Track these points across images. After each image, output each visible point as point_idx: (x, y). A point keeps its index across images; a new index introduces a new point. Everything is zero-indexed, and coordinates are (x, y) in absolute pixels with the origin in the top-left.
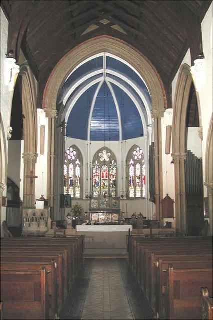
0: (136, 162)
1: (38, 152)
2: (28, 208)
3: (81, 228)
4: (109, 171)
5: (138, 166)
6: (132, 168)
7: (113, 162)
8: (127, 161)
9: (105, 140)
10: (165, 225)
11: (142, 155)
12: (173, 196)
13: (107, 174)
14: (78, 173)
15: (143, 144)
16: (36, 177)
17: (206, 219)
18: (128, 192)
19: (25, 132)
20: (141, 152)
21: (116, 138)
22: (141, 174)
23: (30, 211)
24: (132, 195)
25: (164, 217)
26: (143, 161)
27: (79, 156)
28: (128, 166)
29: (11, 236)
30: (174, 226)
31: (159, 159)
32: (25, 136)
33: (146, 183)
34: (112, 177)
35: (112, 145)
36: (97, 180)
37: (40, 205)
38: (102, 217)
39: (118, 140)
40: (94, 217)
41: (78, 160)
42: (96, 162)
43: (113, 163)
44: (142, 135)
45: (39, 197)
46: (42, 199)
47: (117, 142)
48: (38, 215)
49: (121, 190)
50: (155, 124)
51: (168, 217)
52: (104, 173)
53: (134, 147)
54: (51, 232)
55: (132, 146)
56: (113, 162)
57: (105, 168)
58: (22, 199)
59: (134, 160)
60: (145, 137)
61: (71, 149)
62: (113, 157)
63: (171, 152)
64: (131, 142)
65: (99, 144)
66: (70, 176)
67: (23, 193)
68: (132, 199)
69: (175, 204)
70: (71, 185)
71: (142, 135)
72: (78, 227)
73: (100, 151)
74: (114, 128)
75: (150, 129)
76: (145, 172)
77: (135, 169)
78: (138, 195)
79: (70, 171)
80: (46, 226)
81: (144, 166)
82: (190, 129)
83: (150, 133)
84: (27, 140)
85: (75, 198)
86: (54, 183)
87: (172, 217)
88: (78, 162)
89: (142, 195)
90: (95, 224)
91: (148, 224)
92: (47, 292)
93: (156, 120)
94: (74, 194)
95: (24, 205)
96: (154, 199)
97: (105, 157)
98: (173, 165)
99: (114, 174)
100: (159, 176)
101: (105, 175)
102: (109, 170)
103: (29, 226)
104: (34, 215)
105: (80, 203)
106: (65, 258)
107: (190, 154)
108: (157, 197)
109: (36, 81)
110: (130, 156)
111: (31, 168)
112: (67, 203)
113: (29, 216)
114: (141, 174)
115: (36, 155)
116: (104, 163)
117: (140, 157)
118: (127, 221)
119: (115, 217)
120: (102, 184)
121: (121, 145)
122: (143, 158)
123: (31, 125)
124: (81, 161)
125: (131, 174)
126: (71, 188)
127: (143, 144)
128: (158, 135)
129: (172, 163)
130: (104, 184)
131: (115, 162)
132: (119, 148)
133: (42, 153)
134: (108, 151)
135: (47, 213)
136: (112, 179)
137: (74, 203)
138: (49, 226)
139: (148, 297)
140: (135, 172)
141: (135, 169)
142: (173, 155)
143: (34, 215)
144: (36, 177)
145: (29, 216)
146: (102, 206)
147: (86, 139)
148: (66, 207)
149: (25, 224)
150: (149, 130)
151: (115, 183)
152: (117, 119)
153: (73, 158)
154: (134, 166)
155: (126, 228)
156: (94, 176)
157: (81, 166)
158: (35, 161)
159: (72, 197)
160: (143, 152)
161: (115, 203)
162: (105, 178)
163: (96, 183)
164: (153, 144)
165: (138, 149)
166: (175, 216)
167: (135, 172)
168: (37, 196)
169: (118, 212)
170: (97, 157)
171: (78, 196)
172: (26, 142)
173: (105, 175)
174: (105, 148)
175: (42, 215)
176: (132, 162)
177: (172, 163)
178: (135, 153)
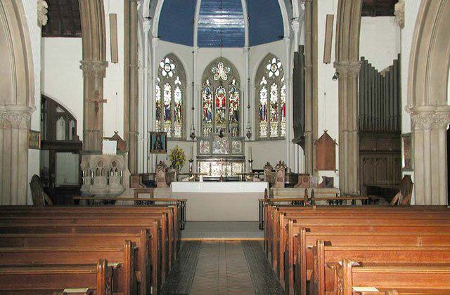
0: (276, 80)
1: (108, 58)
2: (89, 152)
3: (180, 188)
4: (228, 96)
5: (274, 88)
6: (264, 90)
7: (234, 81)
8: (258, 79)
9: (222, 46)
10: (321, 181)
11: (281, 70)
12: (335, 136)
13: (224, 100)
14: (178, 99)
15: (283, 52)
16: (106, 101)
17: (404, 173)
18: (258, 130)
19: (84, 25)
20: (279, 64)
21: (238, 43)
22: (279, 99)
23: (93, 157)
24: (264, 134)
25: (319, 168)
26: (282, 80)
27: (180, 72)
28: (258, 89)
29: (50, 202)
30: (336, 183)
31: (313, 72)
32: (84, 31)
33: (287, 114)
34: (231, 104)
35: (230, 53)
36: (209, 109)
37: (109, 148)
38: (216, 168)
39: (242, 45)
40: (205, 167)
41: (178, 78)
42: (208, 82)
43: (233, 83)
44: (282, 37)
45: (112, 135)
46: (116, 137)
47: (240, 50)
48: (108, 164)
49: (246, 125)
50: (306, 14)
51: (326, 169)
52: (219, 98)
53: (269, 57)
54: (130, 193)
55: (263, 56)
56: (234, 81)
57: (221, 92)
58: (81, 139)
59: (267, 78)
60: (287, 39)
61: (167, 61)
62: (233, 74)
63: (333, 59)
64: (263, 50)
65: (213, 53)
66: (166, 104)
67: (84, 128)
68: (275, 139)
69: (337, 148)
70: (168, 117)
71: (282, 37)
72: (173, 184)
73: (214, 63)
74: (236, 27)
75: (296, 24)
76: (287, 97)
77: (269, 92)
78: (274, 133)
79: (165, 95)
80: (121, 182)
81: (284, 87)
82: (363, 18)
83: (296, 30)
84: (88, 40)
85: (173, 139)
86: (430, 265)
87: (333, 168)
88: (177, 81)
89: (280, 133)
90: (206, 180)
91: (294, 180)
92: (134, 278)
93: (309, 4)
94: (173, 131)
95: (87, 147)
96: (303, 138)
97: (222, 73)
98: (336, 81)
99: (235, 100)
100: (312, 100)
101: (221, 102)
102: (227, 94)
103: (92, 182)
104: (100, 163)
105: (181, 145)
106: (154, 234)
107: (366, 66)
108: (308, 135)
109: (275, 268)
110: (261, 72)
111: (96, 85)
112: (161, 146)
113: (93, 166)
114: (279, 99)
115: (105, 64)
116: (221, 82)
117: (277, 74)
118: (255, 174)
119: (237, 168)
120: (216, 115)
121: (247, 54)
122: (282, 75)
123: (93, 12)
124: (183, 79)
125: (263, 101)
126: (168, 122)
127: (283, 52)
128: (312, 32)
129: (334, 78)
130: (220, 116)
131: (238, 81)
132: (243, 59)
133: (115, 61)
134: (227, 63)
135: (122, 162)
136: (233, 108)
137: (171, 146)
138: (127, 182)
139: (270, 262)
140: (269, 96)
141: (269, 92)
142: (336, 65)
143: (100, 163)
144: (106, 101)
145: (93, 166)
146: (216, 151)
147: (191, 44)
148: (160, 152)
149: (87, 180)
150: (294, 28)
151: (237, 115)
152: (242, 11)
153: (171, 74)
154: (268, 87)
155: (259, 187)
156: (205, 103)
157: (183, 88)
158: (103, 74)
159: (169, 135)
160: (283, 64)
161: (238, 146)
162: (221, 106)
163: (206, 115)
164: (301, 48)
165: (274, 61)
166: (337, 168)
167: (269, 96)
168: (108, 131)
169: (241, 159)
170: (209, 73)
171: (178, 134)
172: (85, 41)
173: (221, 102)
174: (221, 59)
175: (114, 164)
176: (264, 81)
177: (334, 78)
178: (269, 67)
